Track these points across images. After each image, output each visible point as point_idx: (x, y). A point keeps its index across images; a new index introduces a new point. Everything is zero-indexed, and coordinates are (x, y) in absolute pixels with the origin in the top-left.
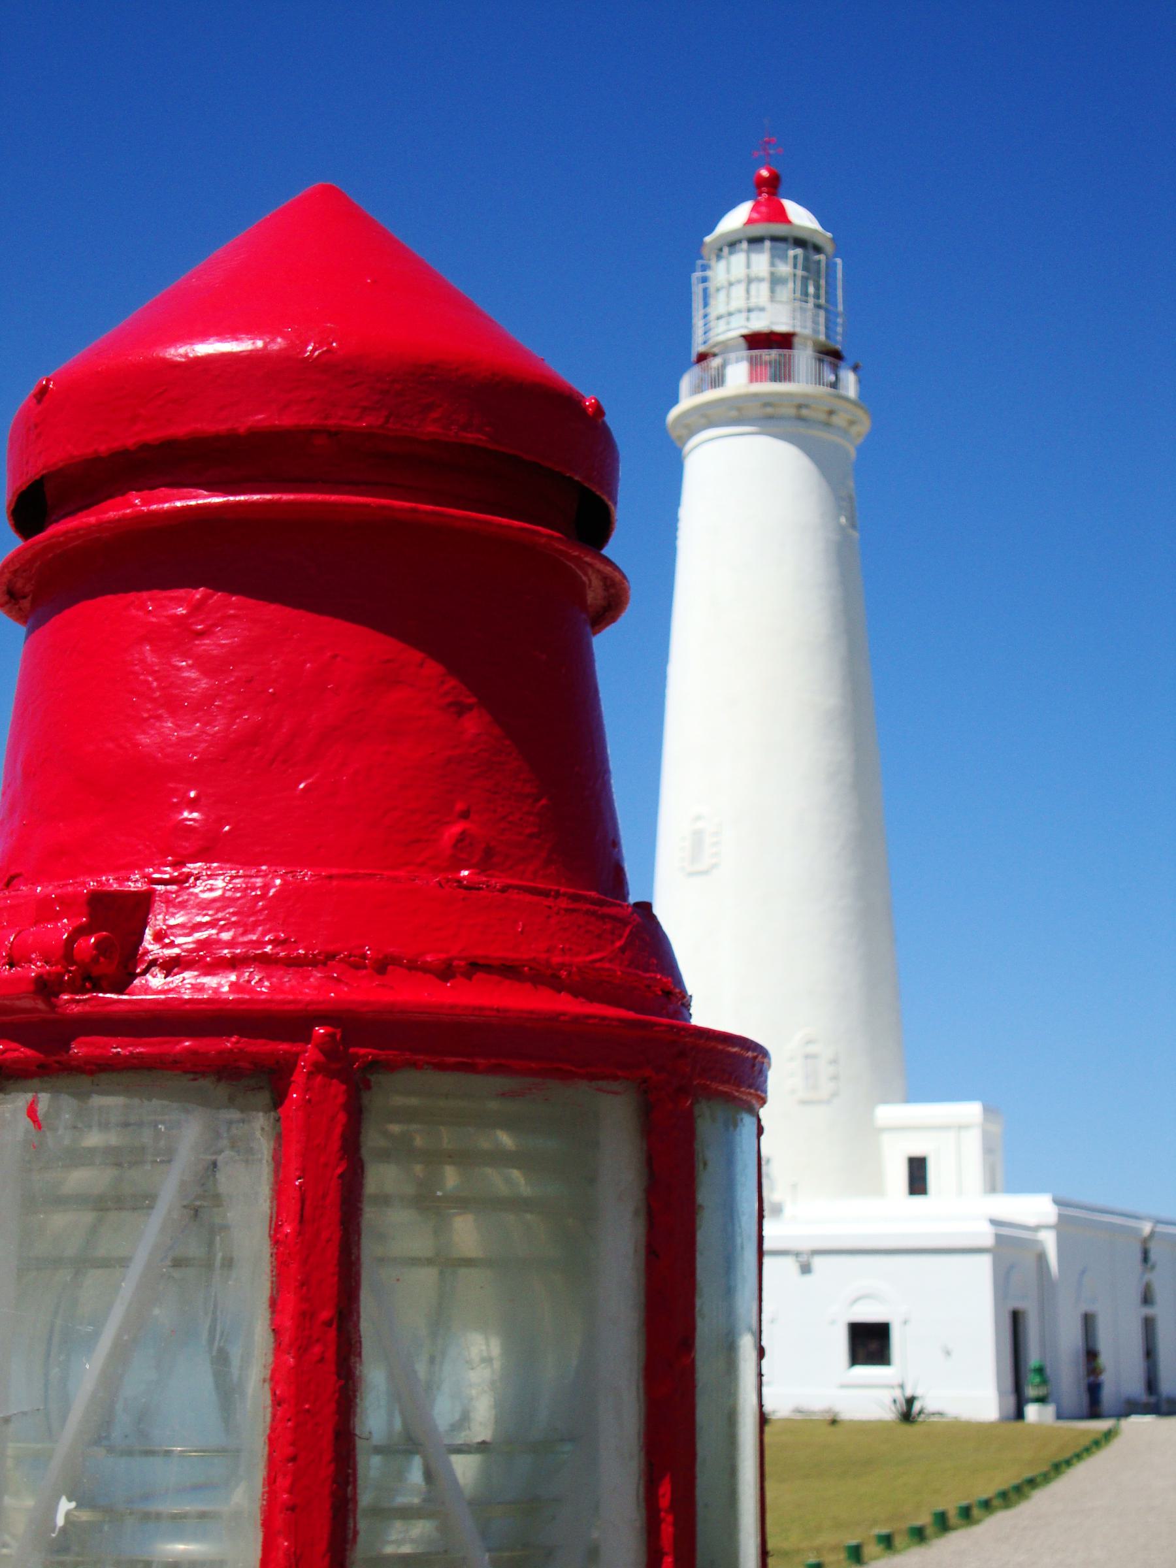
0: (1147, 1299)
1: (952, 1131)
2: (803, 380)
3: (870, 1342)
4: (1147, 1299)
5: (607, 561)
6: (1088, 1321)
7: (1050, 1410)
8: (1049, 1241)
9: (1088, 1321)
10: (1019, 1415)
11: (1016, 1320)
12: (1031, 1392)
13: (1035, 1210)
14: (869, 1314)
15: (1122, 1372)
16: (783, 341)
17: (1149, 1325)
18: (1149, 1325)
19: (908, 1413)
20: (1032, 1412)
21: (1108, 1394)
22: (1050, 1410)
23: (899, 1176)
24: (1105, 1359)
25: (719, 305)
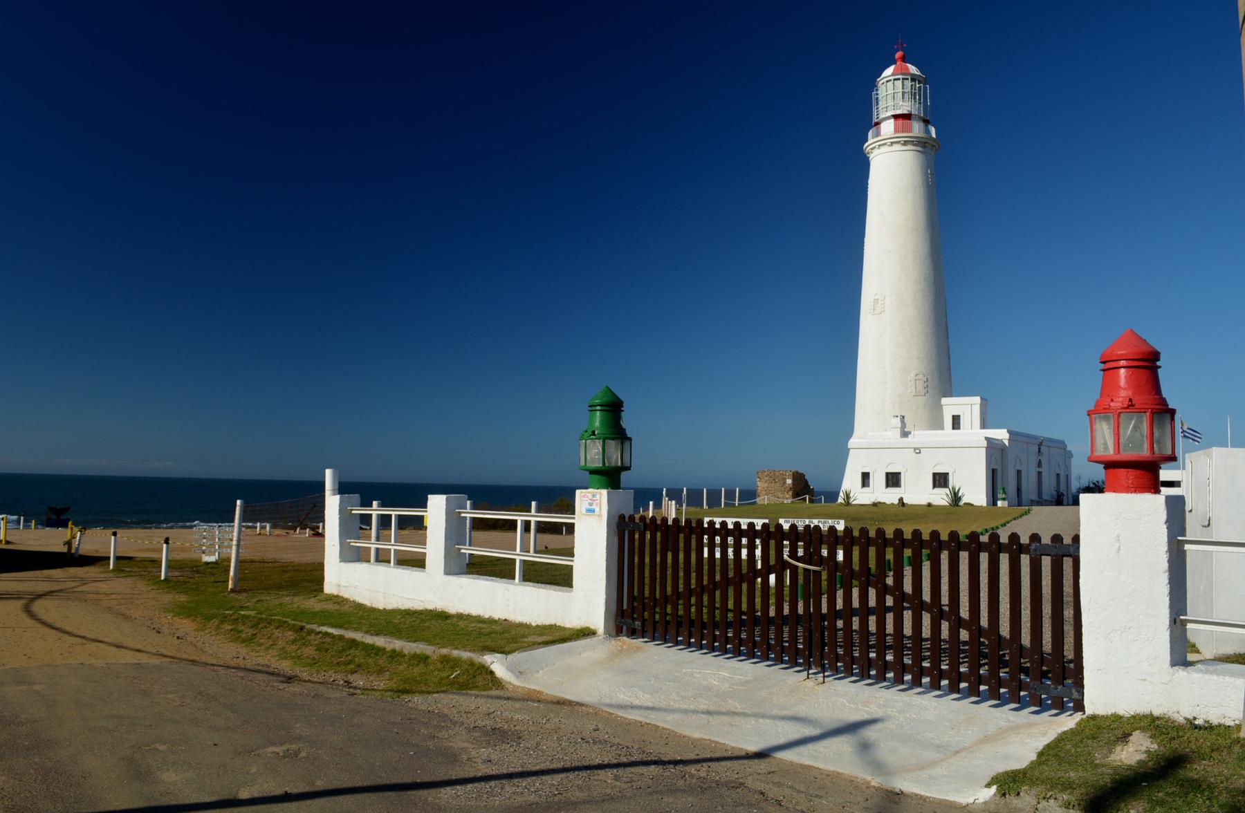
0: (1040, 464)
1: (968, 406)
2: (917, 128)
3: (940, 480)
4: (1040, 464)
5: (337, 600)
6: (1019, 472)
7: (1006, 504)
8: (1006, 443)
9: (1019, 472)
10: (995, 504)
11: (994, 471)
12: (1000, 496)
13: (1002, 435)
14: (941, 469)
15: (1029, 490)
16: (907, 117)
17: (1040, 473)
18: (1040, 473)
19: (901, 500)
20: (1000, 503)
21: (1024, 497)
22: (1006, 504)
23: (948, 422)
24: (1024, 488)
25: (882, 104)
